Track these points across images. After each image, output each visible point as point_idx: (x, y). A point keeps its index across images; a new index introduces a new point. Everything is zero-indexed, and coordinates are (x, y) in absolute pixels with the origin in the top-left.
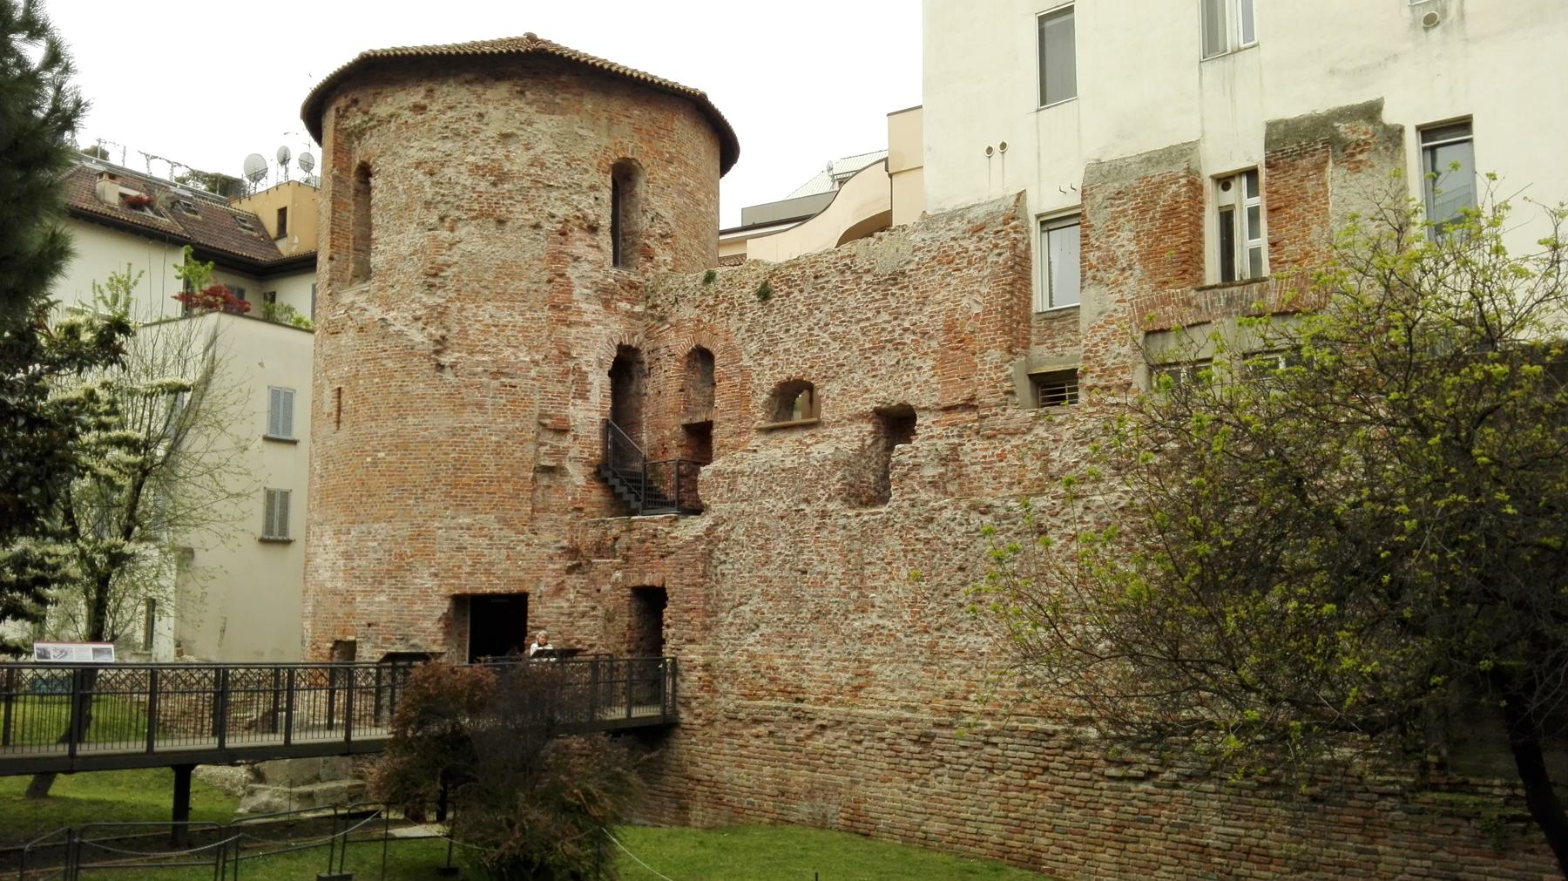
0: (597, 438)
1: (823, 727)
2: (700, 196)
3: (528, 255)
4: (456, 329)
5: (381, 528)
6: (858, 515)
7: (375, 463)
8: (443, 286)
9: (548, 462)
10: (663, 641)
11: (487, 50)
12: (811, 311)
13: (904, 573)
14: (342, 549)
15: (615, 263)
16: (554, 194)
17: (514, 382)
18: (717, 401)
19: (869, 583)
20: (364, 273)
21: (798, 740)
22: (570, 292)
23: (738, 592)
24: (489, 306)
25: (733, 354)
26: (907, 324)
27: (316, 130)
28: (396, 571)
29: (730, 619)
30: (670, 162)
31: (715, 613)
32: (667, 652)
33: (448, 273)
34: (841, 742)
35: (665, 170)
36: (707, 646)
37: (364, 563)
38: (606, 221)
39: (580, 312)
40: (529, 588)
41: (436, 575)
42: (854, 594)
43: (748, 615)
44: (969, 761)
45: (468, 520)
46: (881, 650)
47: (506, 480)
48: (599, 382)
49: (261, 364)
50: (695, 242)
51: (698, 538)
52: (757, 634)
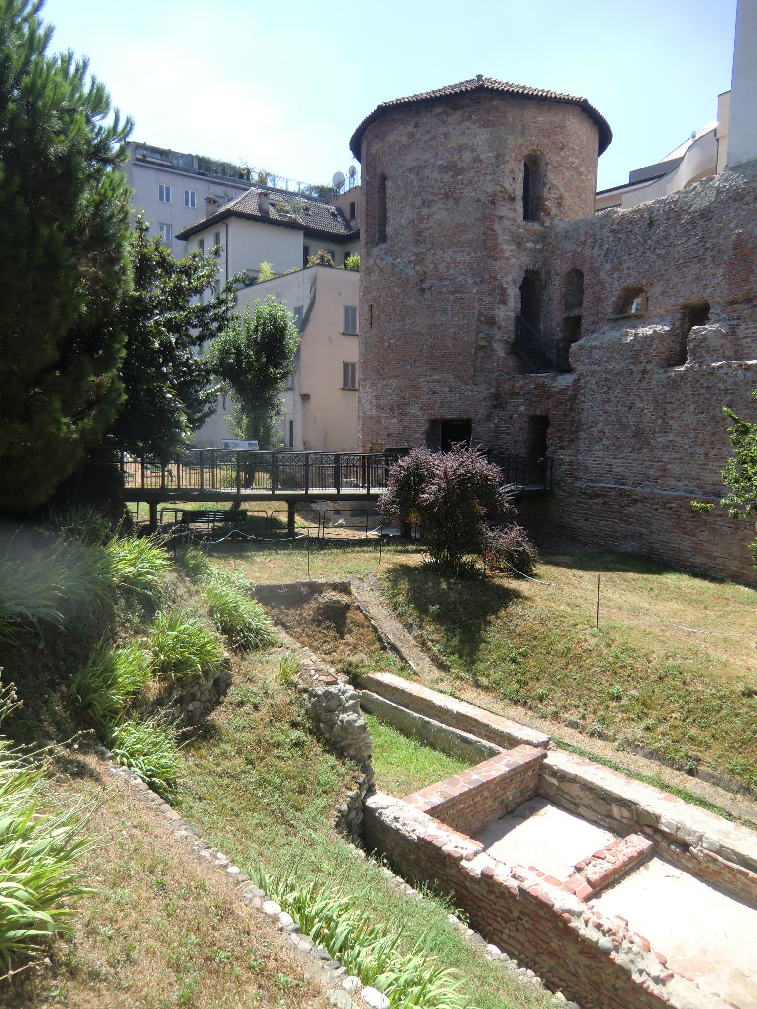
0: (512, 327)
1: (636, 500)
2: (583, 169)
3: (472, 218)
4: (432, 266)
5: (394, 382)
6: (665, 372)
7: (389, 346)
8: (424, 242)
9: (482, 343)
10: (546, 448)
11: (448, 92)
12: (645, 241)
13: (692, 409)
14: (374, 394)
15: (526, 218)
16: (489, 178)
17: (463, 296)
18: (584, 302)
19: (669, 415)
20: (383, 238)
21: (621, 506)
22: (496, 239)
23: (591, 419)
24: (451, 252)
25: (595, 272)
26: (708, 245)
27: (358, 154)
28: (401, 407)
29: (585, 435)
30: (562, 149)
31: (577, 432)
32: (548, 454)
33: (427, 234)
34: (646, 509)
35: (558, 154)
36: (571, 452)
37: (385, 401)
38: (519, 192)
39: (502, 251)
40: (472, 415)
41: (422, 408)
42: (660, 421)
43: (596, 433)
44: (721, 523)
45: (438, 378)
46: (674, 455)
47: (460, 354)
48: (513, 293)
49: (339, 294)
50: (577, 200)
51: (567, 387)
52: (600, 444)
